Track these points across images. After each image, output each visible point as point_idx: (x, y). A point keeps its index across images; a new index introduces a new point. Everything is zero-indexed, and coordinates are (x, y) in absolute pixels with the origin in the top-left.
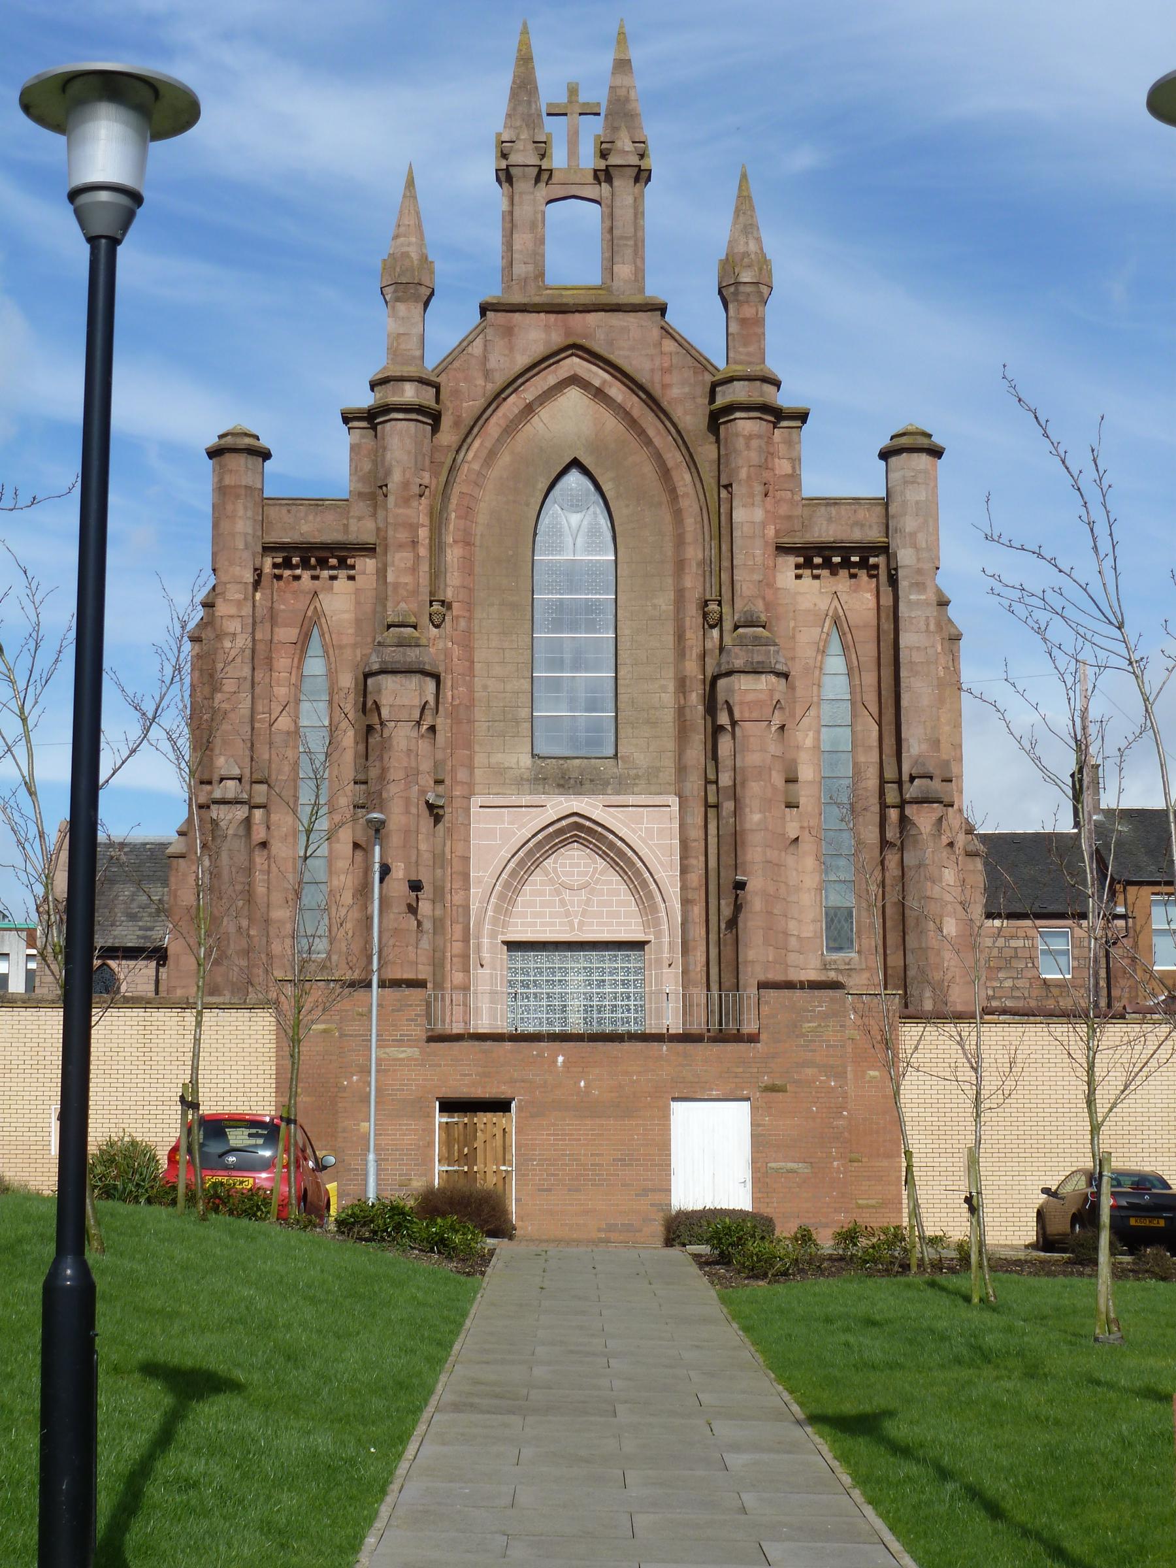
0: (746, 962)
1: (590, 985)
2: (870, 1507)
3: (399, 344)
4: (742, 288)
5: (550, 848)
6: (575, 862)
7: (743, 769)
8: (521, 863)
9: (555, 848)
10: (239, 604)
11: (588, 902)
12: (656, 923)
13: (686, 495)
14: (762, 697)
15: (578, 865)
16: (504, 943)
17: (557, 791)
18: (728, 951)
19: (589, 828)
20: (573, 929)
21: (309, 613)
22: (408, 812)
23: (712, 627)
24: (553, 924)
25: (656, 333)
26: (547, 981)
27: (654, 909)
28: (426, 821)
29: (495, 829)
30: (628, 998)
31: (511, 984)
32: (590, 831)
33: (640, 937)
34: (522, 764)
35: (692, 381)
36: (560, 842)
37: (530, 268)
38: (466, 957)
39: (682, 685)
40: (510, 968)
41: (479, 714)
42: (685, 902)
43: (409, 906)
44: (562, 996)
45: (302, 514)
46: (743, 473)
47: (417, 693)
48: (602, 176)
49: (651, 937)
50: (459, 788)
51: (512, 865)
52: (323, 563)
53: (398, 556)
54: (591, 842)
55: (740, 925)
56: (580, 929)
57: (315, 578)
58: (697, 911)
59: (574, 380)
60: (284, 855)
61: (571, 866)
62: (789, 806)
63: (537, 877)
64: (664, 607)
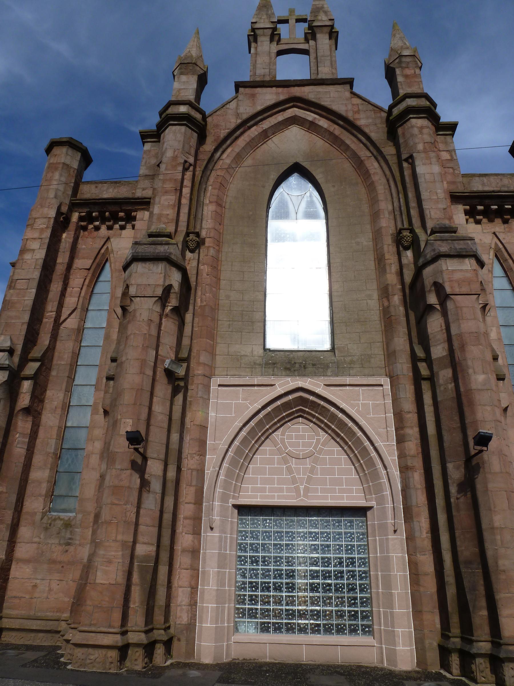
0: (493, 528)
3: (179, 93)
4: (404, 59)
5: (279, 421)
6: (299, 435)
7: (460, 336)
8: (252, 432)
9: (283, 422)
10: (42, 231)
11: (312, 470)
12: (379, 489)
14: (469, 275)
16: (235, 506)
17: (284, 373)
18: (463, 517)
19: (313, 402)
20: (299, 495)
21: (103, 251)
22: (142, 372)
23: (406, 248)
24: (281, 490)
25: (348, 94)
26: (275, 545)
27: (375, 476)
28: (163, 389)
30: (353, 563)
31: (242, 548)
32: (314, 405)
33: (361, 503)
34: (255, 353)
35: (373, 116)
36: (288, 416)
37: (268, 70)
38: (197, 519)
39: (385, 292)
40: (241, 532)
41: (222, 316)
42: (404, 469)
45: (105, 188)
46: (420, 147)
48: (309, 37)
49: (373, 503)
50: (201, 368)
51: (243, 433)
52: (115, 218)
53: (163, 198)
54: (314, 416)
55: (479, 487)
56: (305, 495)
57: (110, 228)
58: (417, 478)
59: (294, 120)
61: (297, 437)
62: (499, 379)
63: (267, 447)
64: (365, 243)
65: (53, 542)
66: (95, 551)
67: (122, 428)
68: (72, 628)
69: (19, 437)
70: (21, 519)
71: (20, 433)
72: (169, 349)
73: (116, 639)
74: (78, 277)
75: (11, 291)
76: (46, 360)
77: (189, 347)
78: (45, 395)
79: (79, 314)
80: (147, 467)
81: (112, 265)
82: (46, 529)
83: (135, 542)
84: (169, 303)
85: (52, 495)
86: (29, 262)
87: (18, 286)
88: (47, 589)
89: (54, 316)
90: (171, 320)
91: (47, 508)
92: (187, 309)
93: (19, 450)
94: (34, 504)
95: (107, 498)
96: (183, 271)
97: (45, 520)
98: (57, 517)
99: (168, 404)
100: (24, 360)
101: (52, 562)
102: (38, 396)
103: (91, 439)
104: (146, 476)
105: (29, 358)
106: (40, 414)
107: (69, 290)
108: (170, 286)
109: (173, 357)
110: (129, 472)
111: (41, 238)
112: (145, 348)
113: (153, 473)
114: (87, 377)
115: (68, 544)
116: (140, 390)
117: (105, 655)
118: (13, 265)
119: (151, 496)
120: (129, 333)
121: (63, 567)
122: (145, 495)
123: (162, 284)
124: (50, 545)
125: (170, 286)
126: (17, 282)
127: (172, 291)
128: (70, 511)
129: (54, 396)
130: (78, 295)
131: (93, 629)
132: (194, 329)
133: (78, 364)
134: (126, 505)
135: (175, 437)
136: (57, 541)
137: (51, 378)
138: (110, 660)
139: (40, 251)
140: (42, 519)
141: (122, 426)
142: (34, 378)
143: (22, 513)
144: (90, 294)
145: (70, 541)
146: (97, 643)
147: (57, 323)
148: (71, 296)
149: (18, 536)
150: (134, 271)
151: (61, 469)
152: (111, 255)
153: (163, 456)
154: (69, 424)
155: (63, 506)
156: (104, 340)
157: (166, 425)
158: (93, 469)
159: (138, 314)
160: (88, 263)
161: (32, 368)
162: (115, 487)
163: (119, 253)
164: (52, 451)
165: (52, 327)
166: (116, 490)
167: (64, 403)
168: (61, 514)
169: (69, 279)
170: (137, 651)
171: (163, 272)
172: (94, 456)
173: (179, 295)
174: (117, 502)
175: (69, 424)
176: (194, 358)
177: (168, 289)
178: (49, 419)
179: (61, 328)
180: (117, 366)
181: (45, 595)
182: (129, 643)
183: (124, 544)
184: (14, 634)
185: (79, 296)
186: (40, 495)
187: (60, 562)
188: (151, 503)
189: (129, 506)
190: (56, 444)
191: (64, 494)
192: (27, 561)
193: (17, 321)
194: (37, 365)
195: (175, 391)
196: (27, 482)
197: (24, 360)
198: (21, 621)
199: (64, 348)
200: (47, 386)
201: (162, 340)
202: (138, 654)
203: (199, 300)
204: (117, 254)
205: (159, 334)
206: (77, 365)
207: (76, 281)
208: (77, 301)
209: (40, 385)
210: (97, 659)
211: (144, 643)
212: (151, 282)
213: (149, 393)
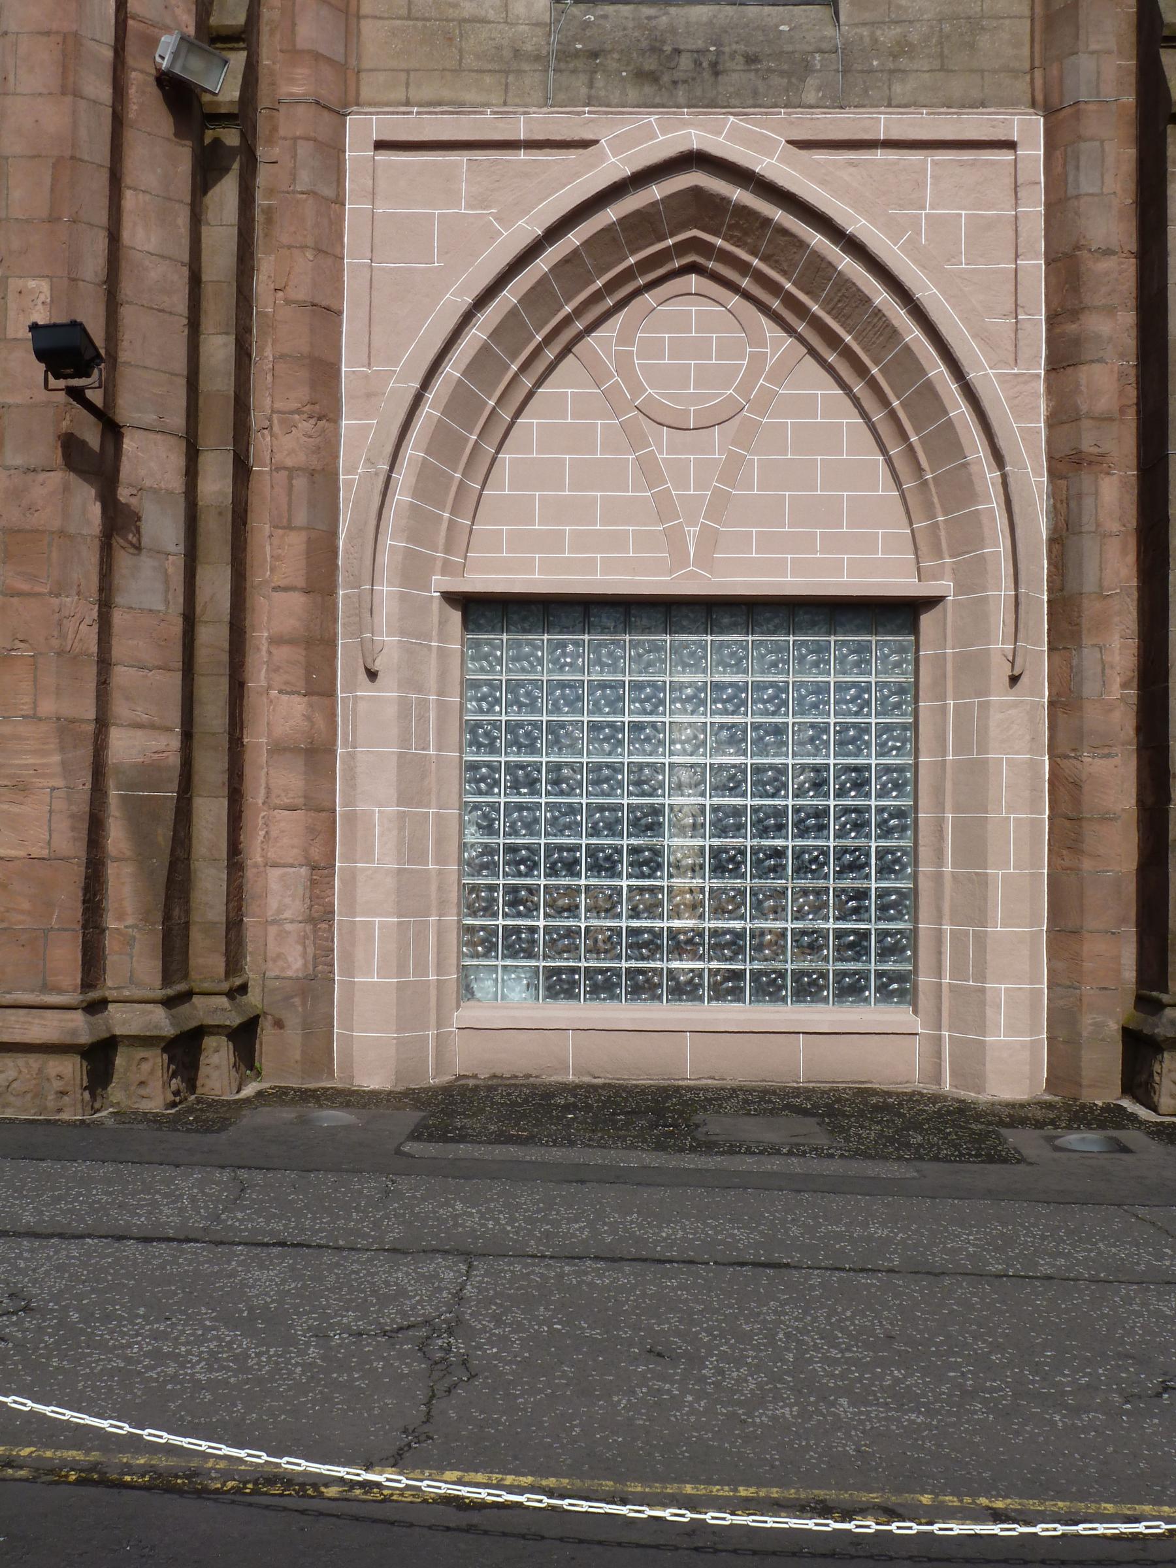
1: (733, 741)
2: (704, 19)
5: (611, 287)
9: (625, 291)
11: (732, 470)
12: (968, 536)
13: (1107, 818)
15: (700, 349)
16: (452, 599)
17: (632, 94)
20: (679, 556)
22: (69, 89)
24: (617, 541)
26: (595, 727)
27: (961, 488)
28: (158, 160)
29: (418, 228)
31: (479, 736)
32: (746, 225)
33: (897, 581)
40: (475, 685)
42: (1067, 465)
43: (71, 447)
44: (641, 781)
49: (943, 586)
50: (301, 72)
51: (477, 334)
54: (744, 268)
56: (705, 560)
63: (566, 386)
73: (71, 1025)
80: (124, 458)
83: (102, 723)
104: (123, 494)
113: (148, 483)
116: (67, 163)
117: (40, 1071)
119: (147, 563)
122: (124, 560)
134: (58, 595)
135: (218, 349)
138: (57, 1085)
153: (178, 421)
157: (180, 304)
174: (25, 587)
176: (272, 33)
183: (65, 727)
195: (207, 168)
202: (146, 1067)
210: (14, 1085)
213: (105, 176)
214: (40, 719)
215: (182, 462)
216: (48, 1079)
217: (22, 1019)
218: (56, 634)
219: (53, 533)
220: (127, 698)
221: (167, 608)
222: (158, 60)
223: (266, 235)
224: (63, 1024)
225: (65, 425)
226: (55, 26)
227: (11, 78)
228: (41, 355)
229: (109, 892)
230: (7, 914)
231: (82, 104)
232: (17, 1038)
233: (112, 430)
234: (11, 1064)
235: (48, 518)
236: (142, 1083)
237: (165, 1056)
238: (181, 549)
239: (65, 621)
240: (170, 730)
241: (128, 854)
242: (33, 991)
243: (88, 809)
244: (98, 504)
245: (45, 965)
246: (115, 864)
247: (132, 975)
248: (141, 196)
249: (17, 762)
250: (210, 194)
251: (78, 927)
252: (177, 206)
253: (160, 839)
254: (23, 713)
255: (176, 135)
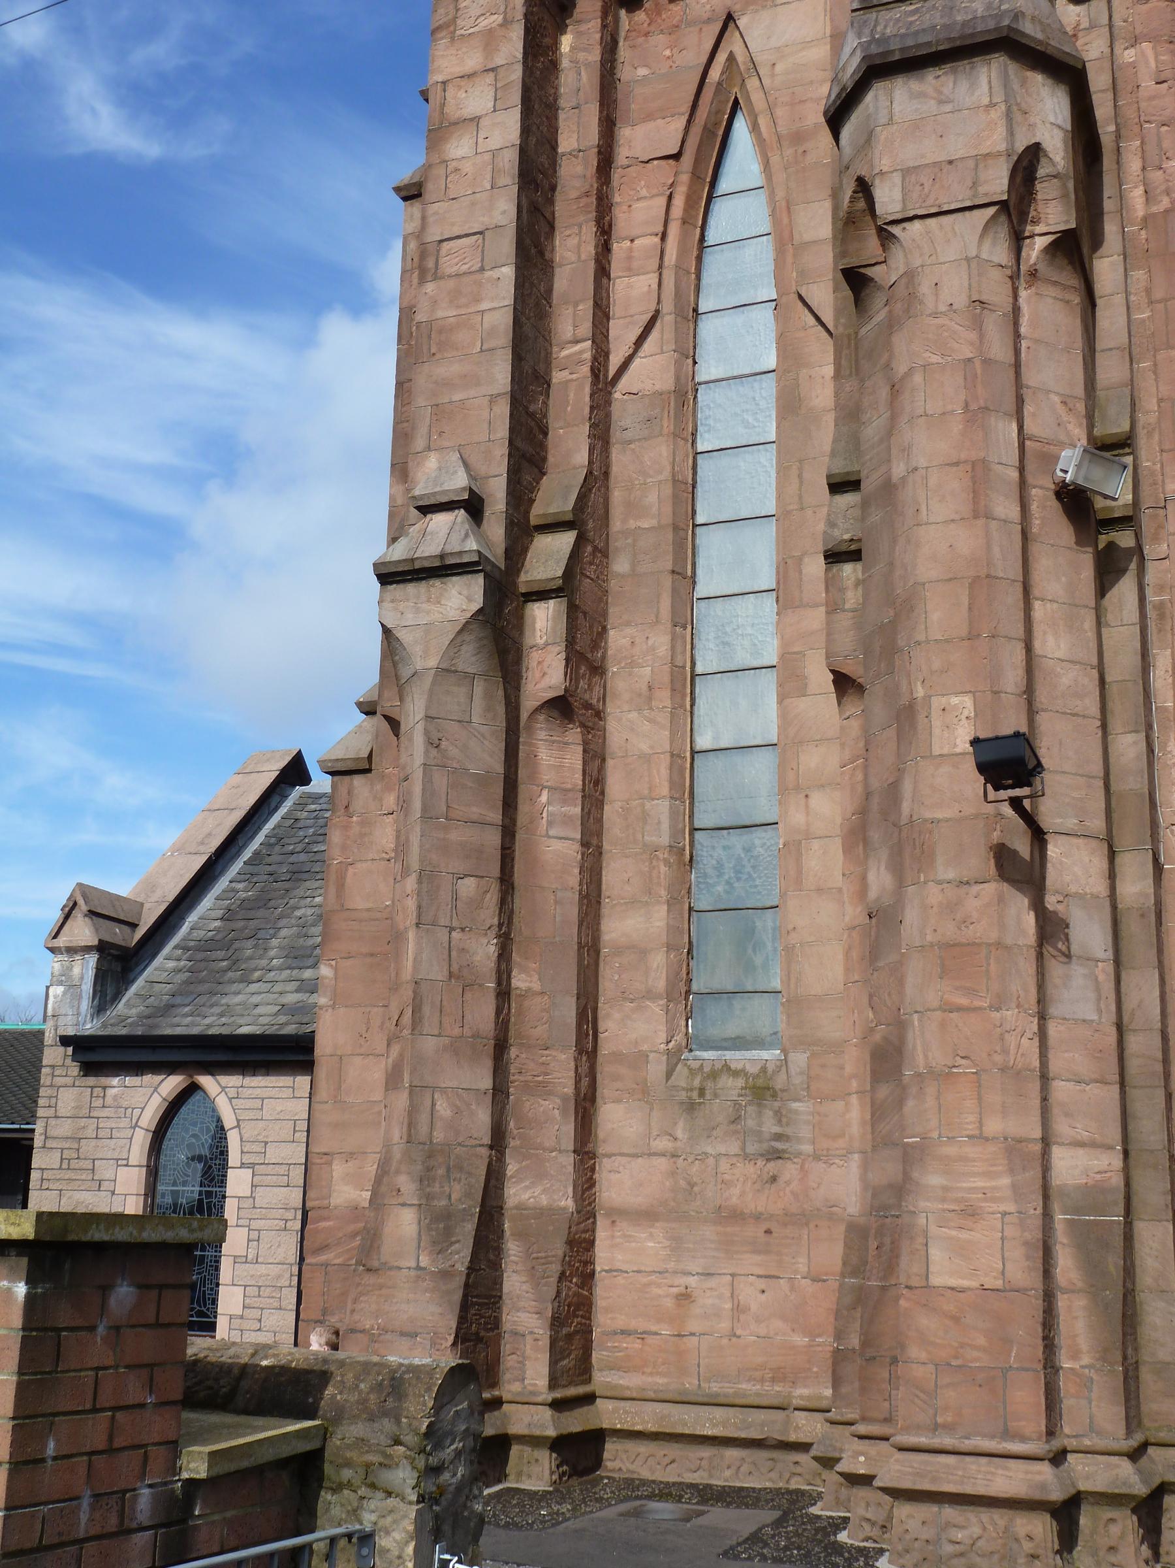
10: (490, 39)
21: (715, 74)
22: (979, 512)
28: (1063, 566)
43: (1003, 856)
47: (997, 114)
60: (644, 747)
65: (722, 1149)
66: (907, 1177)
67: (936, 731)
68: (861, 1437)
69: (549, 803)
70: (599, 1076)
71: (550, 788)
72: (1059, 407)
73: (1038, 1478)
74: (644, 192)
75: (430, 287)
76: (586, 520)
77: (1127, 391)
78: (606, 650)
79: (669, 335)
80: (1049, 865)
81: (763, 122)
82: (690, 1107)
83: (1046, 1142)
84: (1035, 222)
85: (688, 992)
86: (467, 167)
87: (449, 265)
88: (728, 1306)
89: (588, 355)
90: (1052, 291)
91: (679, 1038)
92: (1097, 241)
93: (556, 846)
94: (635, 1027)
95: (922, 987)
96: (1070, 75)
97: (681, 1076)
98: (718, 1066)
99: (1089, 623)
100: (522, 531)
101: (733, 1216)
102: (585, 653)
103: (790, 786)
104: (1051, 901)
105: (533, 521)
106: (599, 715)
107: (619, 248)
108: (1034, 152)
109: (1079, 434)
110: (991, 889)
111: (492, 70)
112: (975, 416)
113: (1073, 889)
114: (739, 563)
115: (776, 1155)
116: (981, 583)
117: (1006, 1529)
118: (411, 193)
119: (1078, 971)
120: (901, 368)
121: (768, 1232)
122: (1056, 969)
123: (1002, 147)
124: (711, 1161)
125: (1034, 152)
126: (443, 252)
127: (1041, 172)
128: (758, 1043)
129: (635, 645)
130: (655, 263)
131: (948, 1442)
132: (1137, 316)
133: (700, 519)
134: (998, 1009)
135: (1127, 746)
136: (734, 1147)
137: (613, 584)
138: (1027, 1546)
139: (501, 116)
140: (669, 1074)
141: (937, 723)
142: (561, 588)
143: (600, 1059)
144: (695, 253)
145: (779, 1145)
146: (969, 1489)
147: (603, 382)
148: (631, 272)
149: (601, 1134)
150: (883, 118)
151: (702, 902)
152: (752, 84)
153: (1097, 824)
154: (702, 742)
155: (732, 1029)
156: (781, 418)
157: (1091, 705)
158: (819, 890)
159: (925, 288)
160: (667, 133)
161: (549, 556)
162: (949, 946)
163: (779, 68)
164: (665, 840)
165: (587, 399)
166: (955, 957)
167: (676, 670)
168: (729, 1055)
169: (610, 207)
170: (1112, 1520)
171: (999, 98)
172: (816, 845)
173: (1071, 185)
174: (964, 1001)
175: (702, 742)
176: (1150, 434)
177: (1026, 167)
178: (635, 730)
179: (617, 395)
180: (865, 505)
181: (725, 1325)
182: (1079, 1493)
183: (1013, 1147)
184: (643, 1448)
185: (661, 267)
186: (649, 995)
187: (758, 1217)
188: (1080, 996)
189: (1009, 1014)
190: (674, 814)
191: (730, 988)
192: (646, 1216)
193: (472, 393)
194: (565, 541)
195: (1109, 567)
196: (598, 952)
197: (522, 531)
198: (658, 1407)
199: (642, 468)
200: (605, 614)
201: (1030, 377)
202: (1115, 1530)
203: (1140, 191)
204: (773, 75)
205: (1017, 352)
206: (695, 526)
207: (640, 210)
208: (655, 286)
209: (585, 613)
210: (980, 1543)
211: (1136, 1492)
212: (957, 147)
213: (1019, 588)
214: (987, 1139)
215: (1105, 865)
216: (1017, 1540)
217: (983, 1469)
218: (998, 1048)
219: (989, 945)
220: (1067, 1115)
221: (1100, 1018)
222: (1060, 474)
223: (1160, 631)
224: (1029, 1476)
225: (996, 837)
226: (963, 456)
227: (923, 508)
228: (982, 768)
229: (1061, 1327)
230: (961, 1351)
231: (994, 524)
232: (981, 1490)
233: (1039, 836)
234: (974, 1520)
235: (982, 930)
236: (1112, 1549)
237: (1135, 1518)
238: (1110, 954)
239: (1007, 1036)
240: (1111, 1148)
241: (1080, 1284)
242: (993, 1437)
243: (1040, 1236)
244: (1032, 914)
245: (1005, 1408)
246: (1065, 1296)
247: (1091, 1421)
248: (1048, 605)
249: (964, 1185)
250: (1108, 596)
251: (1040, 1367)
252: (1083, 611)
253: (1112, 1268)
254: (968, 1132)
255: (1077, 543)
